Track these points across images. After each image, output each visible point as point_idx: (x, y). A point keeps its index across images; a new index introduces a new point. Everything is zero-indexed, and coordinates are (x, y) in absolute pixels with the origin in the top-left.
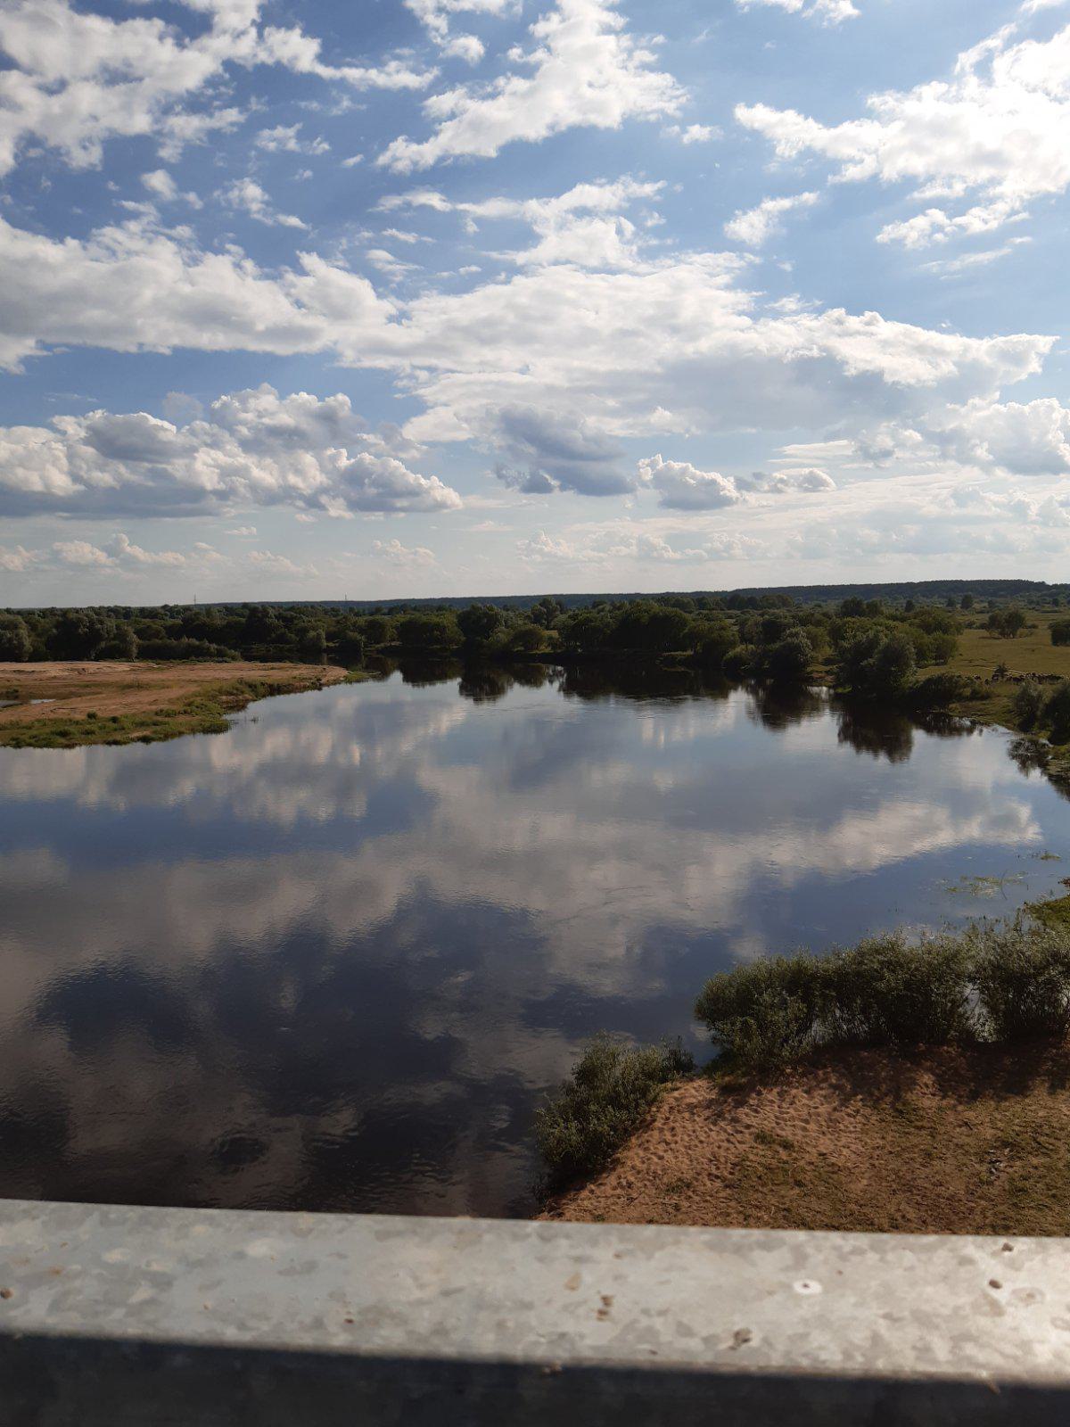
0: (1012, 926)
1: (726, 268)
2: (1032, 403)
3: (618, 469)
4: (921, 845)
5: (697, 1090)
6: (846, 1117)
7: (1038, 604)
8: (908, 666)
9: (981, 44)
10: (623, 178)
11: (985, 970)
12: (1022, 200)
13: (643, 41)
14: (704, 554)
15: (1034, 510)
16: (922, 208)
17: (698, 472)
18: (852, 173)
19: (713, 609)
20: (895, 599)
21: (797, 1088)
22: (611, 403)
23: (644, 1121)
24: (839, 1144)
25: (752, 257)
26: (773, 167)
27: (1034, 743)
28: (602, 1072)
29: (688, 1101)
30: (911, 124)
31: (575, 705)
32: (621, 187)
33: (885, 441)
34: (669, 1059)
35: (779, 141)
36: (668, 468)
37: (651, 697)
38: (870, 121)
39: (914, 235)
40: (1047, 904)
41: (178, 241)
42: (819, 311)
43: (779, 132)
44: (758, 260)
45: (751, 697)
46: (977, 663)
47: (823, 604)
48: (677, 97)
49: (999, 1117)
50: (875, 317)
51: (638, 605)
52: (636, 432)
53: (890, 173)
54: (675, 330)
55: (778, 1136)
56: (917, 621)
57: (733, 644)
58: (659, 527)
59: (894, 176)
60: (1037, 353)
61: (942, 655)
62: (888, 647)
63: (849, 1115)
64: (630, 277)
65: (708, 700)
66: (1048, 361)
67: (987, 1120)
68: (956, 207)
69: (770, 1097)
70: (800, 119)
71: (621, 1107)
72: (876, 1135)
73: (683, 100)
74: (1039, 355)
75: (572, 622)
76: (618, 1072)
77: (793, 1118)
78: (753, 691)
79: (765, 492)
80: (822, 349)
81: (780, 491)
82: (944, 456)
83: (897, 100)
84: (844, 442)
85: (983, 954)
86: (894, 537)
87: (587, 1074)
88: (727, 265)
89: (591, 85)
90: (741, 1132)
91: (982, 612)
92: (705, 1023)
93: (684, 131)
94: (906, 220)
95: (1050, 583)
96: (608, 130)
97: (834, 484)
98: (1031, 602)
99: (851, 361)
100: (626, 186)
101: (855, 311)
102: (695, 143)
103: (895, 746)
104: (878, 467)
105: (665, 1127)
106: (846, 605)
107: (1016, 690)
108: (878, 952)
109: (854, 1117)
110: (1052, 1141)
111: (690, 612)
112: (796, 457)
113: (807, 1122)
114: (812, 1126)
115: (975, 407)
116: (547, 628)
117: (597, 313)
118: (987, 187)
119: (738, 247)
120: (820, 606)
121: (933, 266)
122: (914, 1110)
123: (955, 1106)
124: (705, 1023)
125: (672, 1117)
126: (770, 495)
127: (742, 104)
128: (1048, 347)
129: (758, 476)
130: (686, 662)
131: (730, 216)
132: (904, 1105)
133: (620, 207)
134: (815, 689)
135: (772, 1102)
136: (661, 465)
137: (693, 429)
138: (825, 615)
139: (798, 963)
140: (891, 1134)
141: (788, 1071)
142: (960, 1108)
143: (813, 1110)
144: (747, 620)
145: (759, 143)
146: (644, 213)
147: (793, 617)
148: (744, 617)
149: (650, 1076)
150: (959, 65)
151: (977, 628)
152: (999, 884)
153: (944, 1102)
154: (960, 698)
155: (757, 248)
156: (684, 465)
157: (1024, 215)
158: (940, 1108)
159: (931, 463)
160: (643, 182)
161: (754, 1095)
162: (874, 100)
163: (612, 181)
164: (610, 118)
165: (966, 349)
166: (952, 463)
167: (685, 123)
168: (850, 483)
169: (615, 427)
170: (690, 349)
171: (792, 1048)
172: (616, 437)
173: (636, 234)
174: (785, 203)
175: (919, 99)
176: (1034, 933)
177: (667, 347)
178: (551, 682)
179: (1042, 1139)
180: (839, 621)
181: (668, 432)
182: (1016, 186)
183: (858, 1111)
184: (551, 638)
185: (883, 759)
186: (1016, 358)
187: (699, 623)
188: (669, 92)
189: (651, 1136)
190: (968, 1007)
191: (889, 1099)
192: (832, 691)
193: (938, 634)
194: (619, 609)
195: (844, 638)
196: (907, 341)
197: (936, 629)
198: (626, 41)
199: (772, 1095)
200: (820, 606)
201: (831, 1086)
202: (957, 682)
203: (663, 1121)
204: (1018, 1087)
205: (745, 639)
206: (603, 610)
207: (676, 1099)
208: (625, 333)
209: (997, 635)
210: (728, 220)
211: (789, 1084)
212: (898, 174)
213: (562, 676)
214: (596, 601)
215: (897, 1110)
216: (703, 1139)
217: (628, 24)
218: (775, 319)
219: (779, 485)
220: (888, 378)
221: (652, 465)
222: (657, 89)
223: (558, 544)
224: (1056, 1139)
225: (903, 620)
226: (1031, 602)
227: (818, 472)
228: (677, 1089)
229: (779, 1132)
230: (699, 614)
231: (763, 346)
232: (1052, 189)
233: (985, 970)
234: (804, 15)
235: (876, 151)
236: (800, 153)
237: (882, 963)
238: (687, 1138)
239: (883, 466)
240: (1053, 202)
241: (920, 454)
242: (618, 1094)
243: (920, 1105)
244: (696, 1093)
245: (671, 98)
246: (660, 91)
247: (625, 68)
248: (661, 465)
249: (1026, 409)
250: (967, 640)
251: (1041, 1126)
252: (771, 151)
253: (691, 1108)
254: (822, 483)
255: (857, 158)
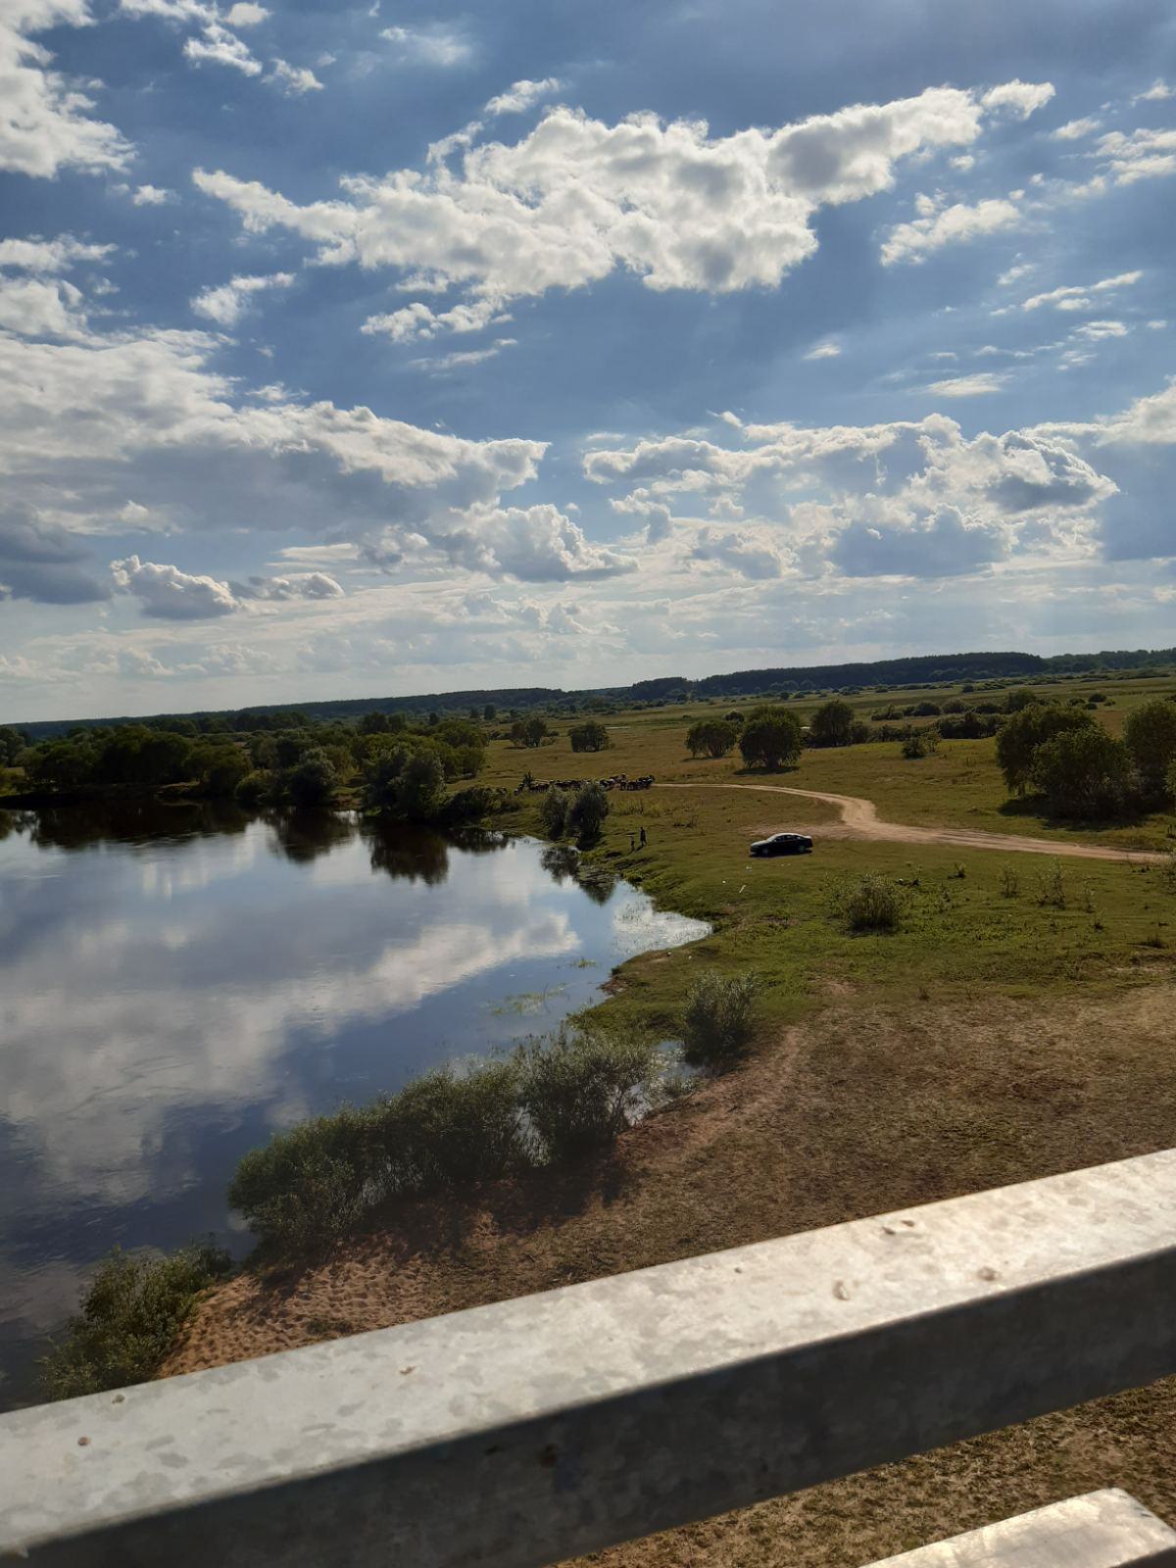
0: (557, 1040)
1: (197, 347)
2: (533, 509)
3: (85, 572)
4: (470, 967)
5: (236, 1291)
6: (406, 1280)
7: (556, 711)
8: (437, 782)
9: (450, 138)
10: (63, 236)
11: (533, 1089)
12: (504, 301)
13: (78, 83)
14: (201, 669)
15: (544, 617)
16: (405, 301)
17: (185, 576)
18: (329, 257)
19: (219, 732)
20: (419, 712)
21: (351, 1260)
22: (69, 495)
23: (176, 1341)
24: (402, 1311)
25: (225, 337)
26: (241, 241)
27: (564, 850)
28: (118, 1296)
29: (227, 1306)
30: (388, 211)
31: (55, 856)
32: (60, 246)
33: (389, 545)
34: (200, 1262)
35: (246, 214)
36: (148, 572)
37: (152, 838)
38: (343, 204)
39: (399, 329)
40: (588, 1013)
41: (960, 150)
42: (307, 403)
43: (244, 204)
44: (233, 342)
45: (271, 828)
46: (505, 774)
47: (343, 721)
48: (123, 152)
49: (559, 1242)
50: (366, 412)
51: (126, 731)
52: (103, 529)
53: (369, 260)
54: (142, 414)
55: (333, 1319)
56: (442, 734)
57: (245, 771)
58: (145, 639)
59: (374, 265)
60: (531, 459)
61: (470, 769)
62: (414, 763)
63: (409, 1277)
64: (80, 350)
65: (221, 837)
66: (542, 466)
67: (548, 1248)
68: (442, 303)
69: (321, 1278)
70: (267, 193)
71: (145, 1332)
72: (439, 1292)
73: (131, 156)
74: (534, 461)
75: (42, 756)
76: (138, 1291)
77: (349, 1296)
78: (271, 821)
79: (267, 599)
80: (312, 443)
81: (283, 598)
82: (453, 562)
83: (371, 184)
84: (347, 546)
85: (531, 1074)
86: (411, 647)
87: (100, 1304)
88: (199, 344)
89: (14, 125)
90: (292, 1326)
91: (505, 722)
92: (242, 1210)
93: (135, 191)
94: (390, 312)
95: (566, 689)
96: (41, 180)
97: (341, 590)
98: (551, 710)
99: (346, 458)
100: (67, 246)
101: (344, 404)
102: (148, 206)
103: (431, 868)
104: (386, 572)
105: (202, 1343)
106: (367, 720)
107: (542, 798)
108: (425, 1091)
109: (415, 1278)
110: (611, 1255)
111: (192, 737)
112: (297, 560)
113: (364, 1296)
114: (371, 1299)
115: (477, 512)
116: (10, 765)
117: (42, 389)
118: (470, 285)
119: (208, 325)
120: (339, 723)
121: (422, 363)
122: (476, 1255)
123: (515, 1241)
124: (242, 1210)
125: (209, 1329)
126: (270, 602)
127: (200, 168)
128: (542, 452)
129: (256, 581)
130: (188, 795)
131: (197, 292)
132: (465, 1252)
133: (60, 268)
134: (343, 814)
135: (325, 1282)
136: (139, 567)
137: (175, 528)
138: (347, 732)
139: (341, 1119)
140: (454, 1286)
141: (340, 1244)
142: (521, 1242)
143: (370, 1282)
144: (259, 742)
145: (223, 215)
146: (92, 278)
147: (312, 736)
148: (255, 738)
149: (178, 1287)
150: (430, 155)
151: (502, 738)
152: (542, 999)
153: (505, 1239)
154: (492, 811)
155: (231, 329)
156: (167, 567)
157: (507, 317)
158: (500, 1247)
159: (440, 569)
160: (87, 243)
161: (303, 1280)
162: (346, 181)
163: (49, 238)
164: (44, 164)
165: (464, 451)
166: (460, 569)
167: (136, 182)
168: (358, 590)
169: (78, 523)
170: (162, 437)
171: (342, 1217)
172: (80, 535)
173: (83, 302)
174: (258, 283)
175: (394, 186)
176: (579, 1044)
177: (134, 433)
178: (20, 831)
179: (601, 1256)
180: (360, 738)
181: (143, 529)
182: (496, 286)
183: (418, 1271)
184: (14, 777)
185: (420, 882)
186: (512, 462)
187: (203, 748)
188: (115, 146)
189: (186, 1357)
190: (521, 1133)
191: (447, 1250)
192: (361, 815)
193: (464, 747)
194: (102, 736)
195: (367, 757)
196: (403, 440)
197: (461, 743)
198: (55, 80)
199: (324, 1275)
200: (339, 723)
201: (386, 1249)
202: (486, 795)
203: (198, 1337)
204: (575, 1208)
205: (258, 765)
206: (81, 739)
207: (213, 1307)
208: (79, 415)
209: (521, 745)
210: (195, 295)
211: (342, 1258)
212: (378, 263)
213: (34, 822)
214: (72, 730)
215: (458, 1259)
216: (248, 1345)
217: (56, 59)
218: (257, 408)
219: (282, 592)
220: (387, 479)
221: (129, 568)
222: (98, 140)
223: (16, 662)
224: (615, 1252)
225: (427, 734)
226: (551, 710)
227: (323, 576)
228: (213, 1295)
229: (335, 1315)
230: (202, 738)
231: (246, 437)
232: (533, 292)
233: (533, 1089)
234: (264, 81)
235: (353, 236)
236: (270, 230)
237: (429, 1102)
238: (228, 1349)
239: (391, 571)
240: (534, 305)
241: (429, 559)
242: (140, 1318)
243: (482, 1248)
244: (236, 1295)
245: (117, 152)
246: (102, 143)
247: (57, 111)
248: (139, 567)
249: (527, 514)
250: (493, 750)
251: (599, 1243)
252: (238, 222)
253: (232, 1313)
254: (331, 589)
255: (333, 242)
